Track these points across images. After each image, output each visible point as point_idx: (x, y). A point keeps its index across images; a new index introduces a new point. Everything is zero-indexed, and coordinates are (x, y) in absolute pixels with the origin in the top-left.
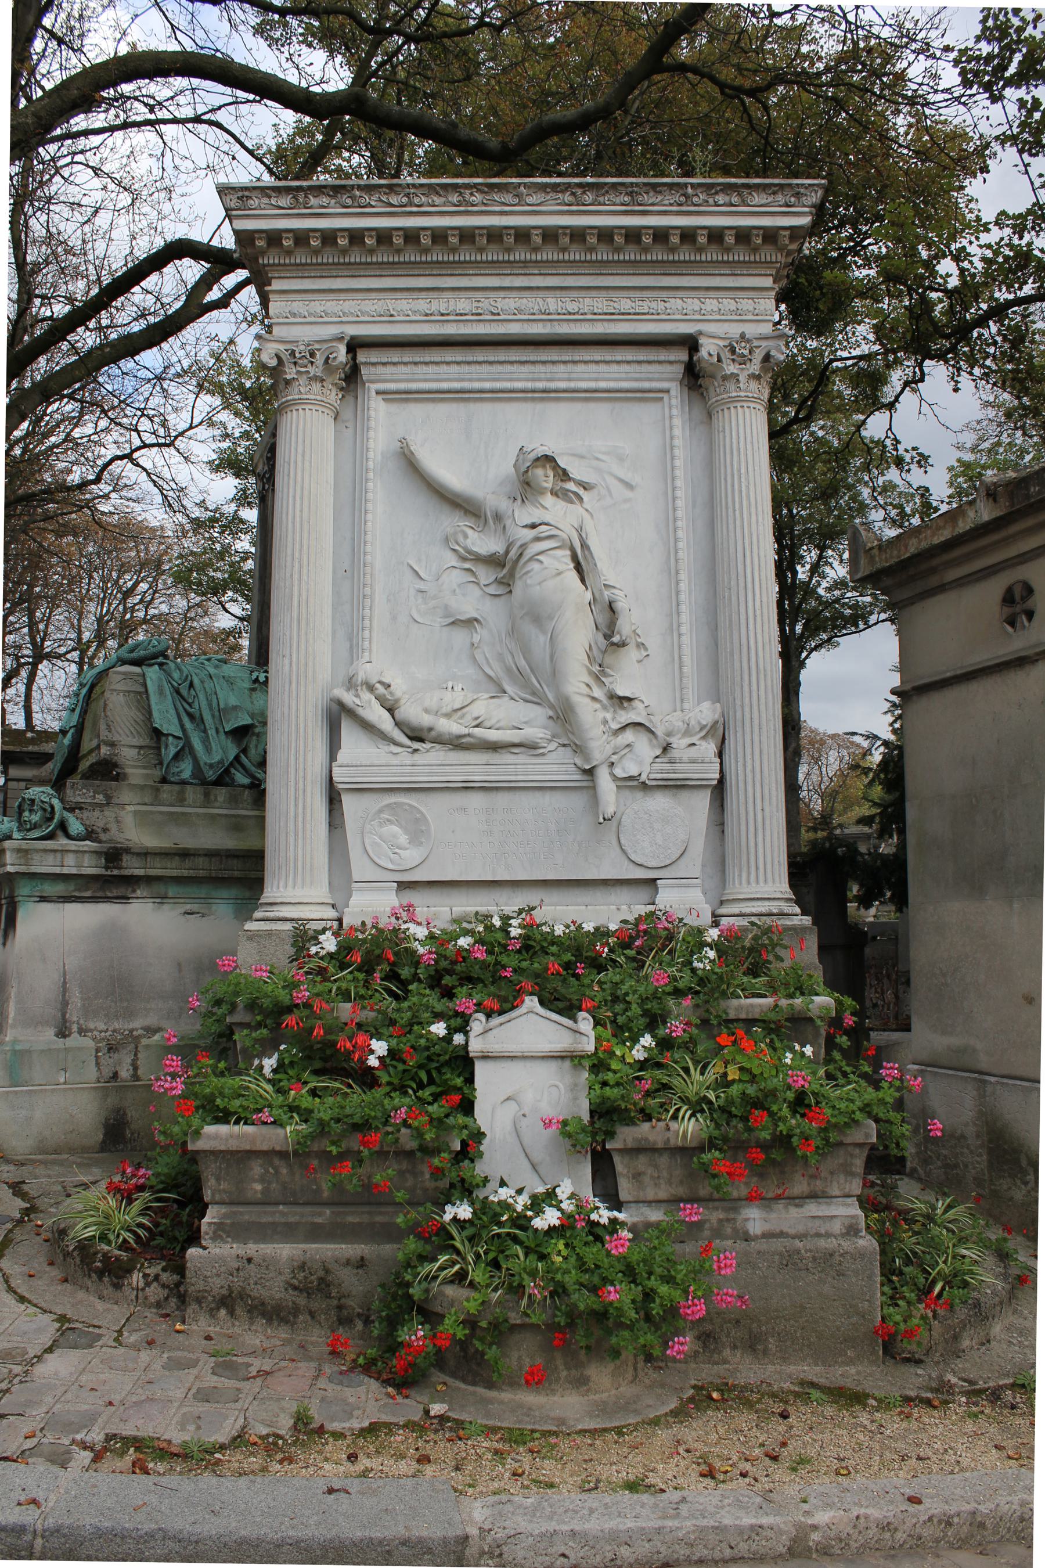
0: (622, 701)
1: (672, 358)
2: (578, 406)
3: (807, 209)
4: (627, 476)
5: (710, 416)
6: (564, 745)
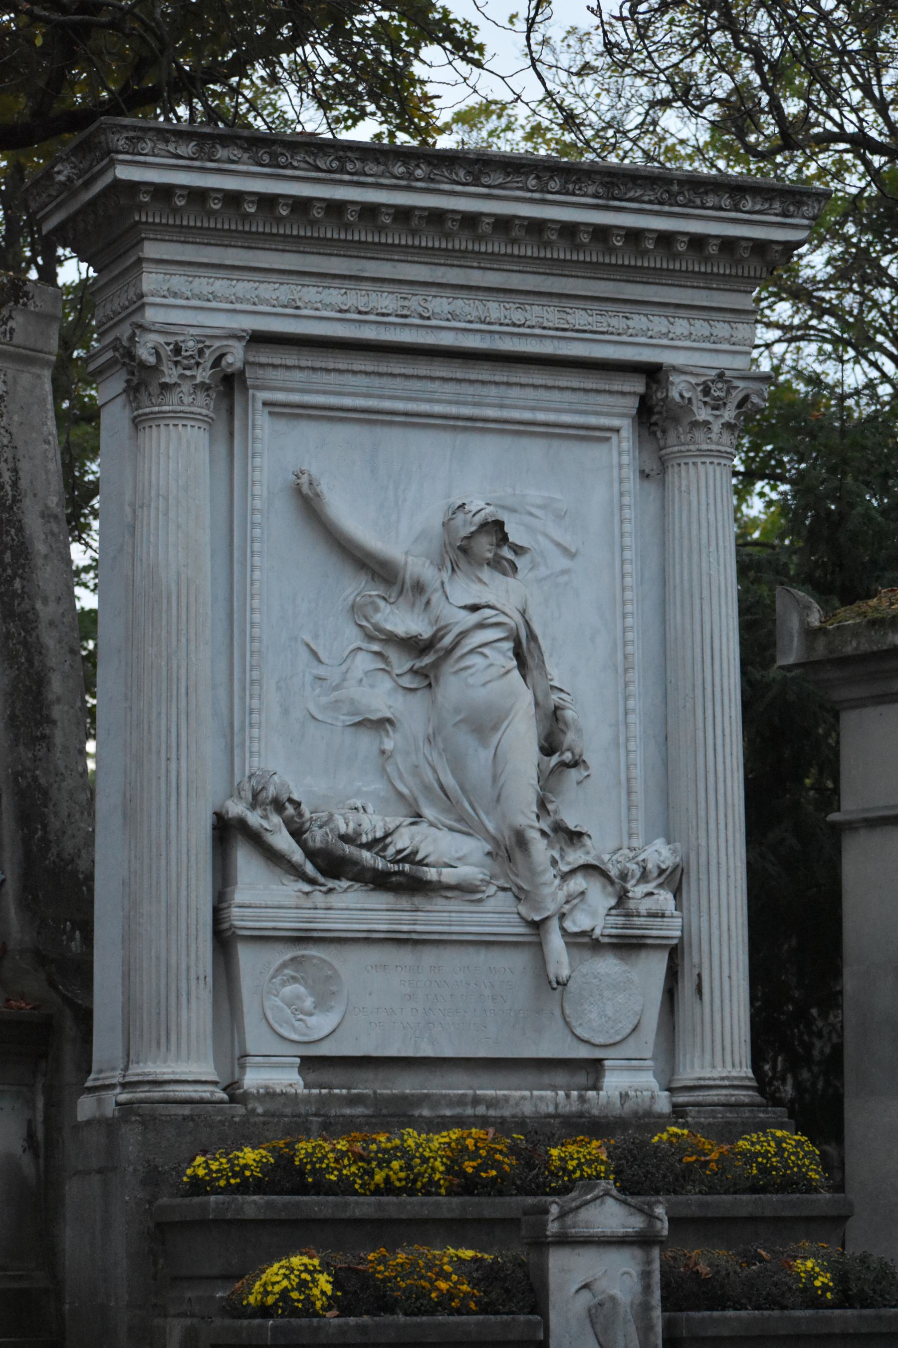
0: (574, 837)
1: (627, 388)
2: (508, 441)
3: (805, 222)
4: (566, 540)
5: (663, 464)
6: (504, 889)
